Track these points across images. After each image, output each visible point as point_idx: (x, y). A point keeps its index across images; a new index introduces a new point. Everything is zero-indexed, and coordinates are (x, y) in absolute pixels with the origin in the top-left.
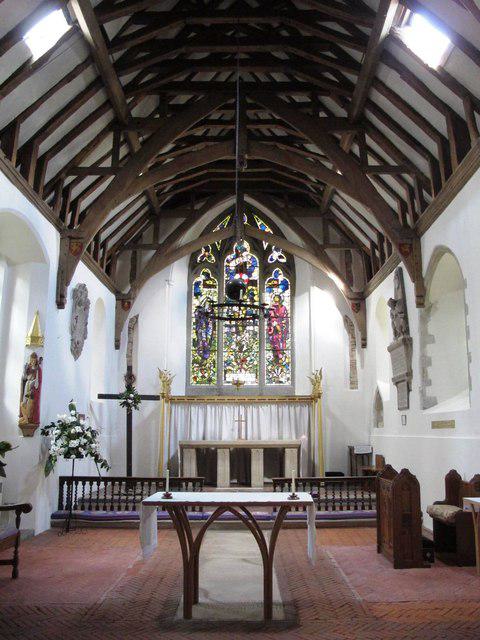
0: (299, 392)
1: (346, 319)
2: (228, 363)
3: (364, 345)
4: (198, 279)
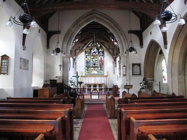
2: (92, 70)
3: (116, 67)
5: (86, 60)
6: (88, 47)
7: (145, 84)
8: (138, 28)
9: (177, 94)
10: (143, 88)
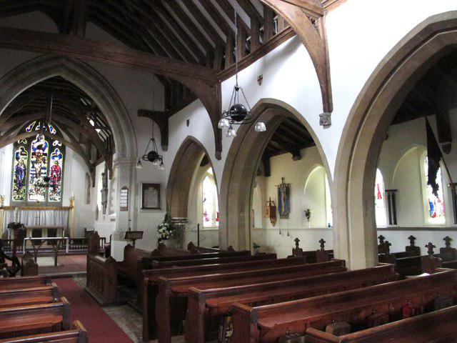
0: (64, 205)
1: (87, 174)
2: (31, 191)
3: (94, 186)
4: (18, 151)
5: (15, 165)
6: (23, 131)
7: (168, 230)
8: (160, 107)
9: (236, 249)
10: (165, 239)
